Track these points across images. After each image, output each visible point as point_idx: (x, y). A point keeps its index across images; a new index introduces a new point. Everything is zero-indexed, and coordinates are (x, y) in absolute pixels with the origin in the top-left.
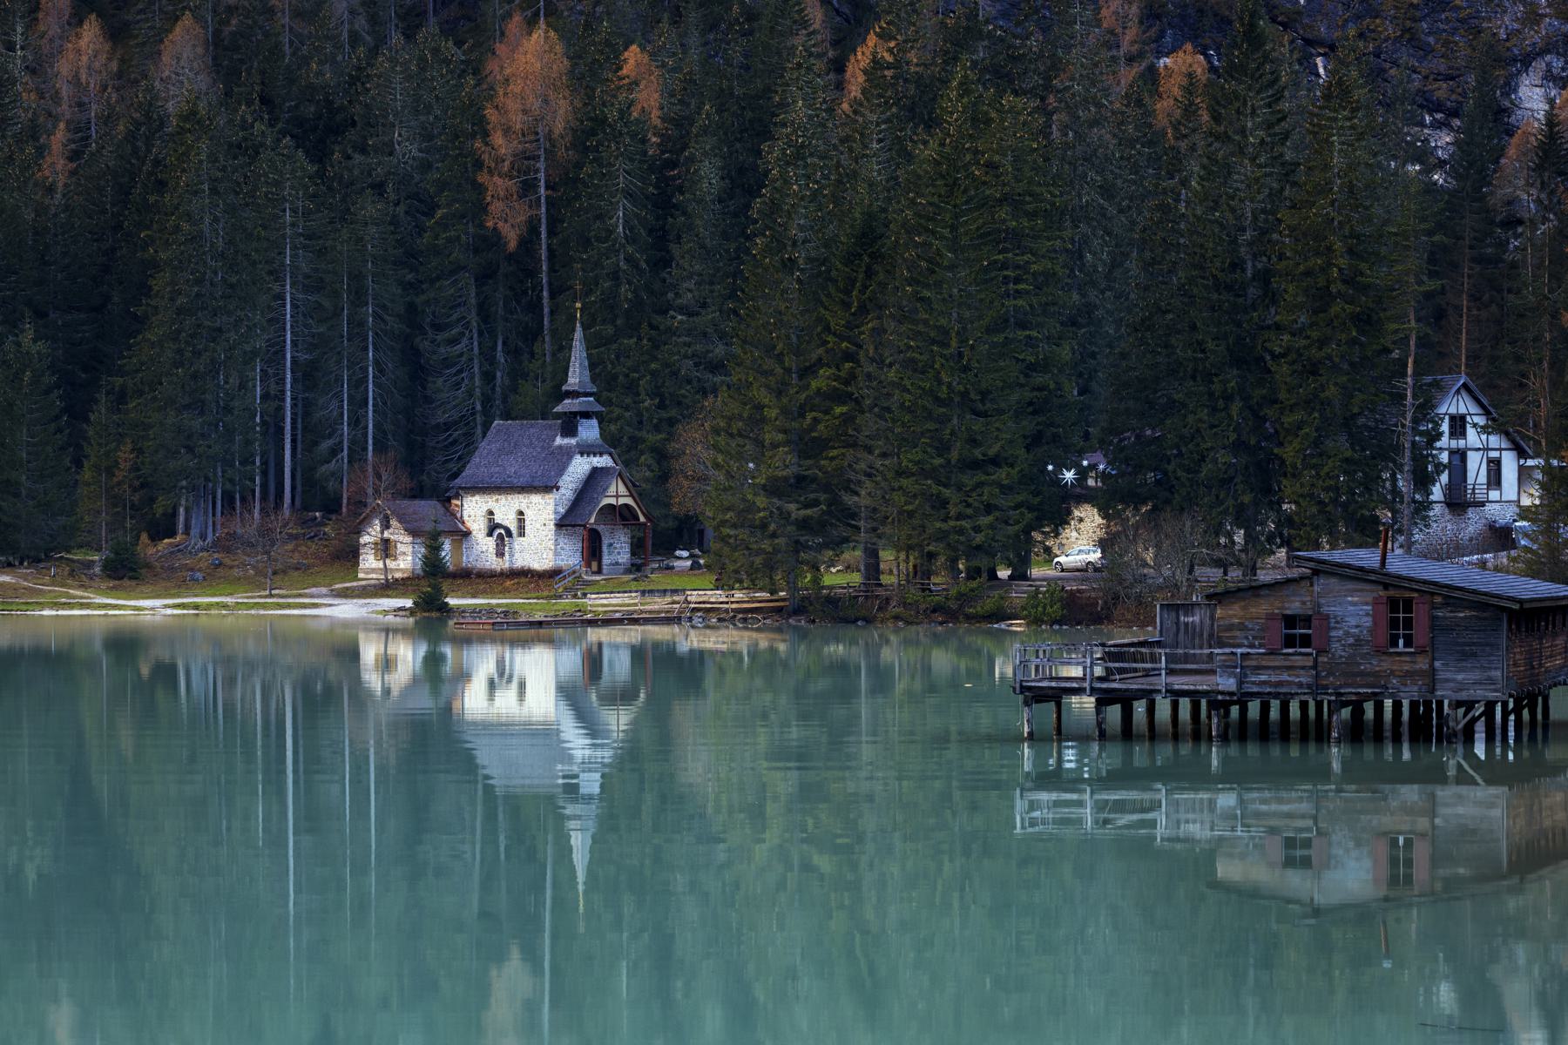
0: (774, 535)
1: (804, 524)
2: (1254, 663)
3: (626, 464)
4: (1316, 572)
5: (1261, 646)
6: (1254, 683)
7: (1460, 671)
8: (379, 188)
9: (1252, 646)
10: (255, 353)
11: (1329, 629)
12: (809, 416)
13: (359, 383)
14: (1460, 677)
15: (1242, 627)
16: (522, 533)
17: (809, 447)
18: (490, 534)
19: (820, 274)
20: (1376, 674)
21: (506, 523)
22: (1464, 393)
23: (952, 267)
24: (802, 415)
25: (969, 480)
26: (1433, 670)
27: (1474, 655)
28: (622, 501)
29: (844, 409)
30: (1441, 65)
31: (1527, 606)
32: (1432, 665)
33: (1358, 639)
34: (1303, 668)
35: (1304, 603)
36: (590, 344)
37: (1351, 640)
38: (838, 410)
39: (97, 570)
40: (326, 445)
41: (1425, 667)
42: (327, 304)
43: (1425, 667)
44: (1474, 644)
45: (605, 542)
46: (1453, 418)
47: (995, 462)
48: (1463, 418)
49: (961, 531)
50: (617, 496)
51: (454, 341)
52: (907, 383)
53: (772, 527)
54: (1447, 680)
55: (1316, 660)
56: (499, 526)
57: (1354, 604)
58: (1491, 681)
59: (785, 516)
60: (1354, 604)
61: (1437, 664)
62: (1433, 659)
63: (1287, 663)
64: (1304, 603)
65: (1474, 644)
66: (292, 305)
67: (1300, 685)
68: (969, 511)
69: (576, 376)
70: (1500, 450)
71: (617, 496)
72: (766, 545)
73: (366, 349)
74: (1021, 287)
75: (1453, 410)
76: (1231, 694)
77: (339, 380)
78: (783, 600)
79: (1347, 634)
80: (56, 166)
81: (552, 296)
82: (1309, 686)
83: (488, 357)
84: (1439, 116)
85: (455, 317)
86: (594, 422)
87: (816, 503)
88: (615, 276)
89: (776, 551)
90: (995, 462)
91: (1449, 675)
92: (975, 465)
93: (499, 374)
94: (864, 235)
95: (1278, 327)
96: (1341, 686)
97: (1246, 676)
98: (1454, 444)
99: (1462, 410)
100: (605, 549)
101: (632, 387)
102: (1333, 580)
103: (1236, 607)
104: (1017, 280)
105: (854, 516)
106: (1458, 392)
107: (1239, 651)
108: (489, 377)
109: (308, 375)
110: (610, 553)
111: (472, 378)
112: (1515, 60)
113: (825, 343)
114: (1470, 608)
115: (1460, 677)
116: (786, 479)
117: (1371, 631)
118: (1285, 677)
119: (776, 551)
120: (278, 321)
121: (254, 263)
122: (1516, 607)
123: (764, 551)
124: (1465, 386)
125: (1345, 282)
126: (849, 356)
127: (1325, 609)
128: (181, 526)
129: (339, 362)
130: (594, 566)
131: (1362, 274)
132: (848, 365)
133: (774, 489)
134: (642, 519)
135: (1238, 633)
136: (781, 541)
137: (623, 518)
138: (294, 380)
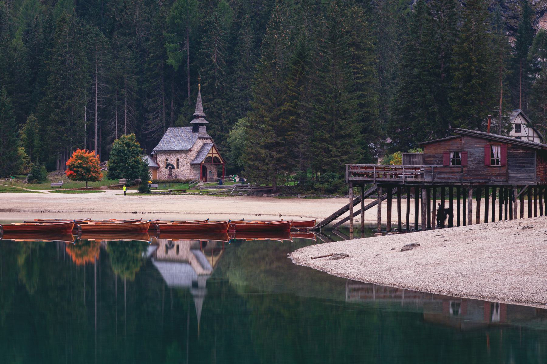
0: (267, 164)
1: (279, 160)
2: (439, 171)
3: (217, 144)
4: (463, 135)
5: (441, 164)
6: (438, 178)
7: (518, 173)
8: (130, 47)
9: (438, 164)
10: (84, 104)
11: (467, 157)
12: (281, 120)
13: (121, 117)
14: (518, 176)
15: (434, 157)
16: (178, 167)
17: (280, 131)
18: (166, 168)
19: (285, 69)
20: (486, 175)
21: (173, 163)
22: (520, 116)
23: (334, 65)
24: (278, 120)
25: (338, 143)
26: (508, 173)
27: (524, 167)
28: (214, 155)
29: (294, 117)
30: (511, 14)
31: (544, 149)
32: (507, 171)
33: (479, 161)
34: (458, 172)
35: (458, 147)
36: (204, 101)
37: (476, 162)
38: (291, 118)
39: (27, 180)
40: (109, 138)
41: (505, 172)
42: (110, 88)
43: (505, 172)
44: (524, 163)
45: (208, 170)
46: (516, 125)
47: (350, 136)
48: (520, 125)
49: (336, 161)
50: (213, 154)
51: (155, 102)
52: (317, 107)
53: (267, 160)
54: (513, 177)
55: (462, 170)
56: (170, 164)
57: (478, 148)
58: (530, 177)
59: (271, 156)
60: (478, 148)
61: (509, 171)
62: (508, 169)
63: (451, 171)
64: (458, 147)
65: (524, 163)
66: (98, 88)
67: (457, 179)
68: (339, 154)
69: (199, 111)
70: (533, 137)
71: (213, 154)
72: (264, 168)
73: (124, 104)
74: (360, 75)
75: (516, 122)
76: (430, 182)
77: (114, 114)
78: (271, 187)
79: (475, 159)
80: (18, 41)
81: (191, 84)
82: (460, 179)
83: (168, 107)
84: (511, 32)
85: (156, 93)
86: (205, 127)
87: (283, 152)
88: (214, 78)
89: (269, 169)
90: (350, 136)
91: (514, 175)
92: (342, 137)
93: (172, 113)
94: (301, 54)
95: (453, 88)
96: (472, 180)
97: (435, 175)
98: (517, 134)
99: (520, 122)
100: (208, 173)
101: (219, 116)
102: (469, 138)
103: (432, 149)
104: (357, 73)
105: (298, 157)
106: (518, 115)
107: (433, 166)
108: (168, 114)
109: (103, 113)
110: (210, 175)
111: (162, 114)
112: (538, 13)
113: (287, 93)
114: (523, 149)
115: (518, 176)
116: (272, 143)
117: (484, 158)
118: (450, 176)
119: (269, 169)
120: (92, 94)
121: (84, 72)
122: (540, 148)
123: (264, 170)
124: (520, 113)
125: (477, 71)
126: (296, 98)
127: (466, 150)
128: (58, 167)
129: (114, 108)
130: (204, 179)
131: (483, 68)
132: (295, 101)
133: (267, 147)
134: (222, 162)
135: (432, 159)
136: (270, 166)
137: (215, 162)
138: (98, 115)
